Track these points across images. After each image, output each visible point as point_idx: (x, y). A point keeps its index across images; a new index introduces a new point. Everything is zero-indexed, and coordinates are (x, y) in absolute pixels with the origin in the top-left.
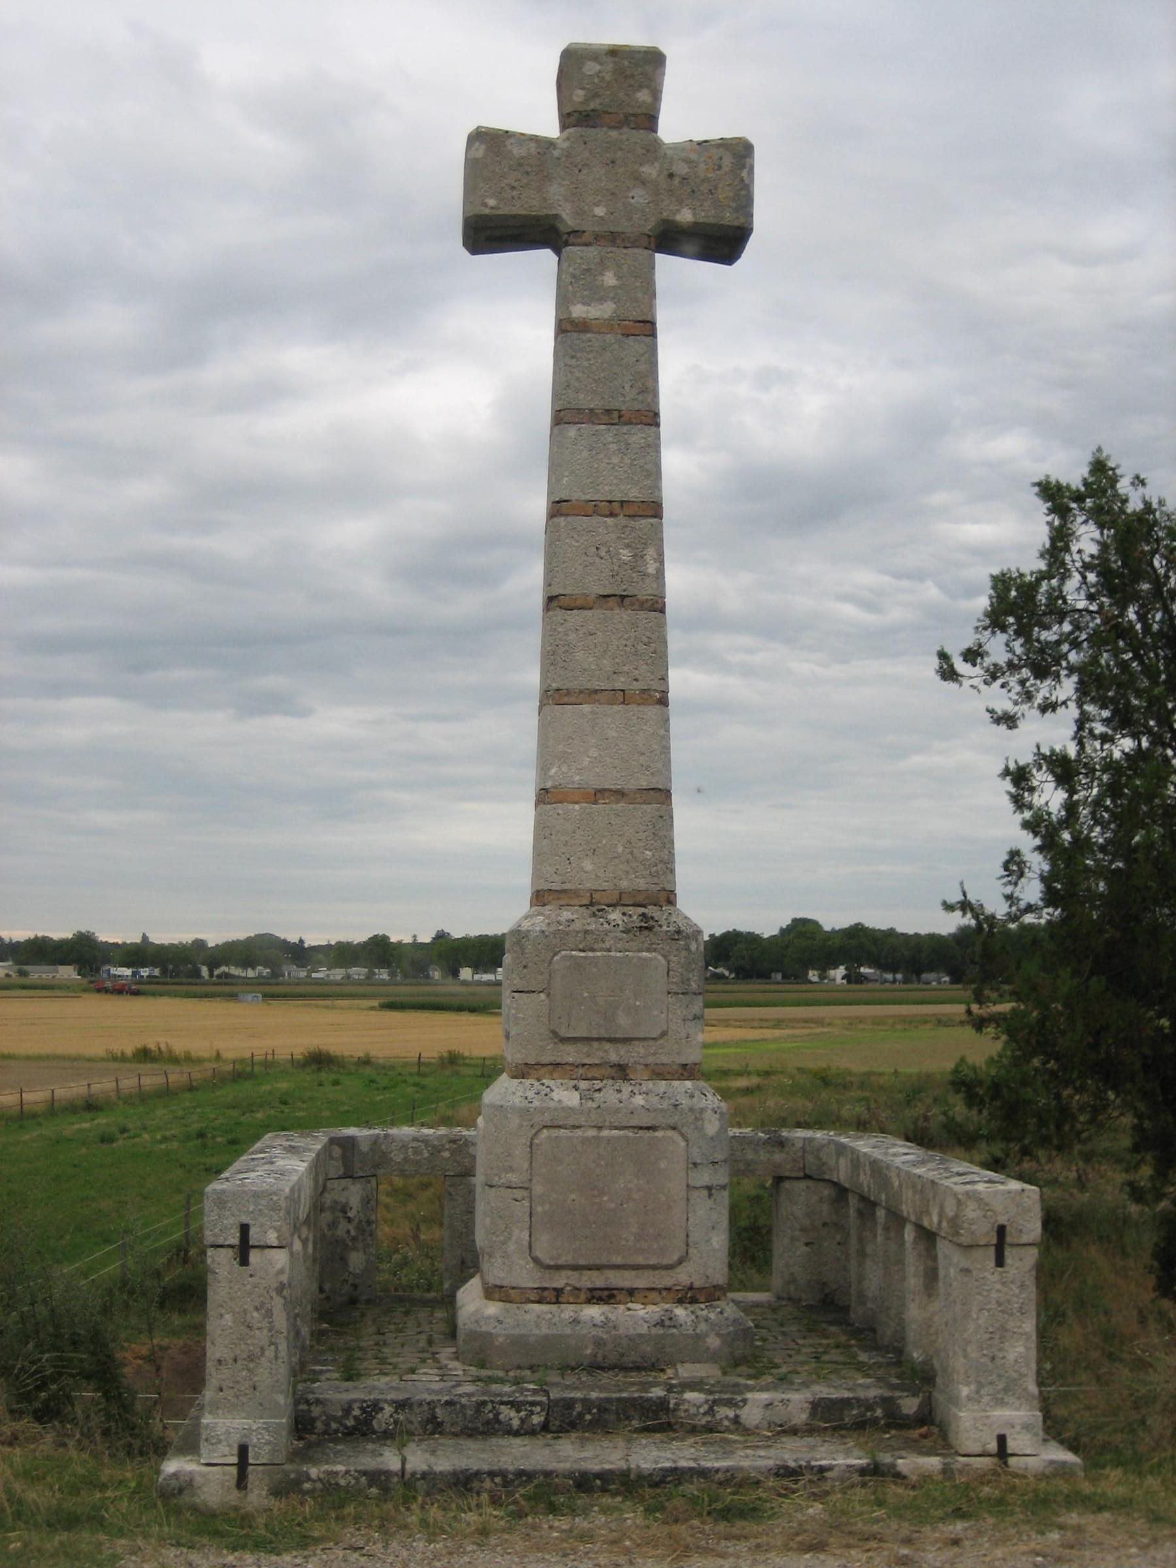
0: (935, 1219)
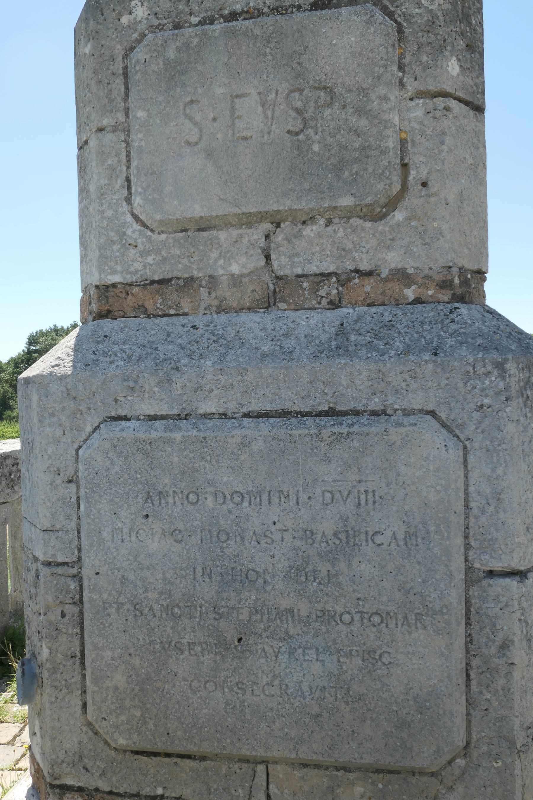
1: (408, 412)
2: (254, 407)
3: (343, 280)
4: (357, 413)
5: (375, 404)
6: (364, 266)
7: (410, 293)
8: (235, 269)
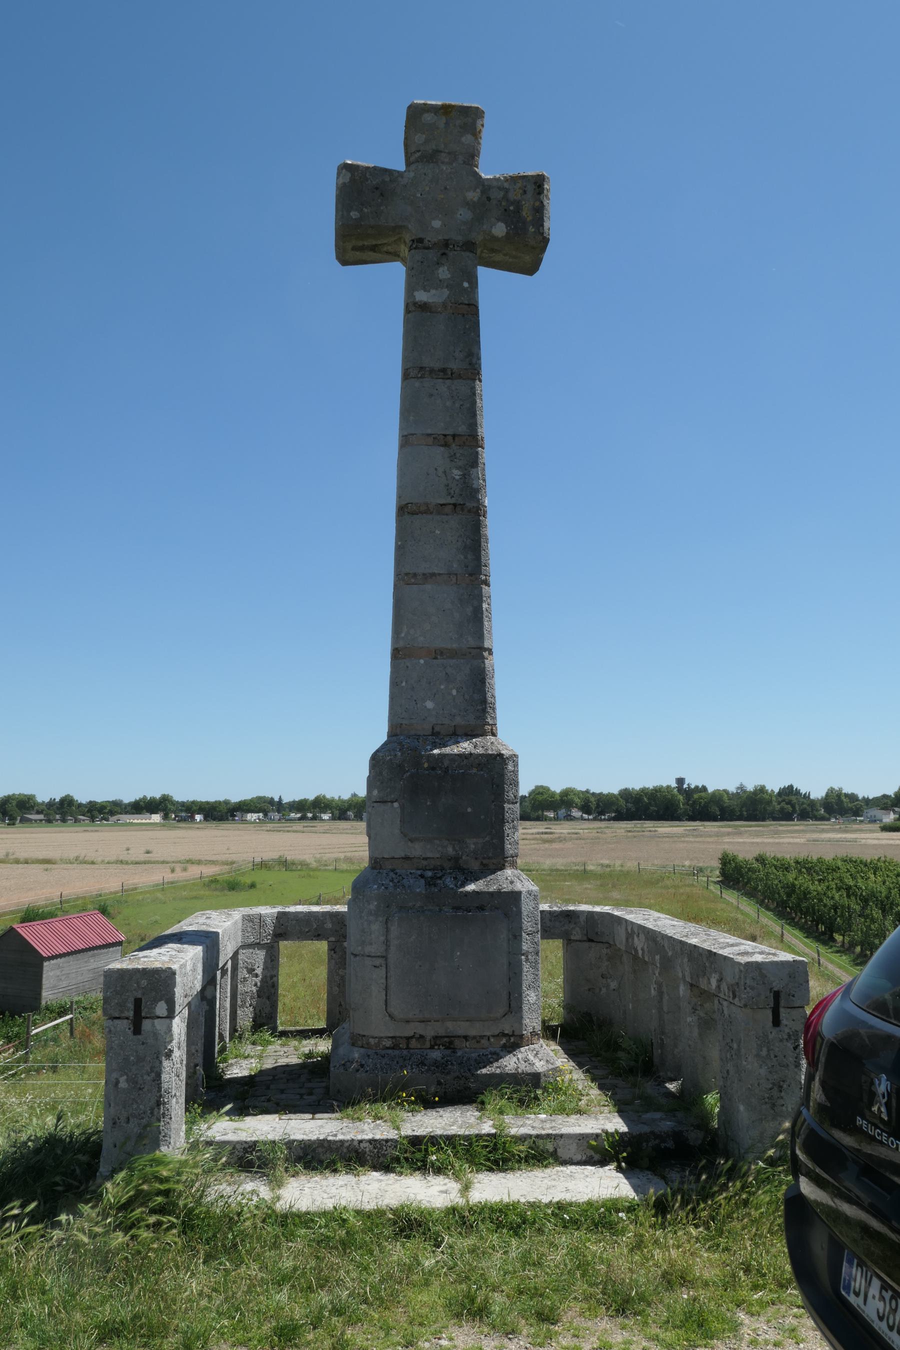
0: (714, 983)
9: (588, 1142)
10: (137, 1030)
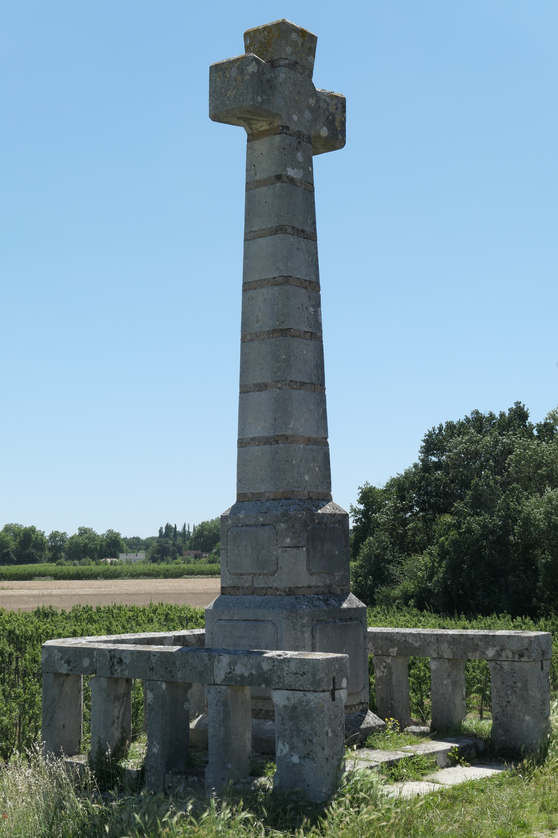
1: (268, 621)
2: (243, 619)
3: (266, 589)
4: (260, 621)
5: (263, 619)
6: (270, 586)
7: (278, 593)
8: (247, 585)
9: (447, 754)
10: (333, 699)
